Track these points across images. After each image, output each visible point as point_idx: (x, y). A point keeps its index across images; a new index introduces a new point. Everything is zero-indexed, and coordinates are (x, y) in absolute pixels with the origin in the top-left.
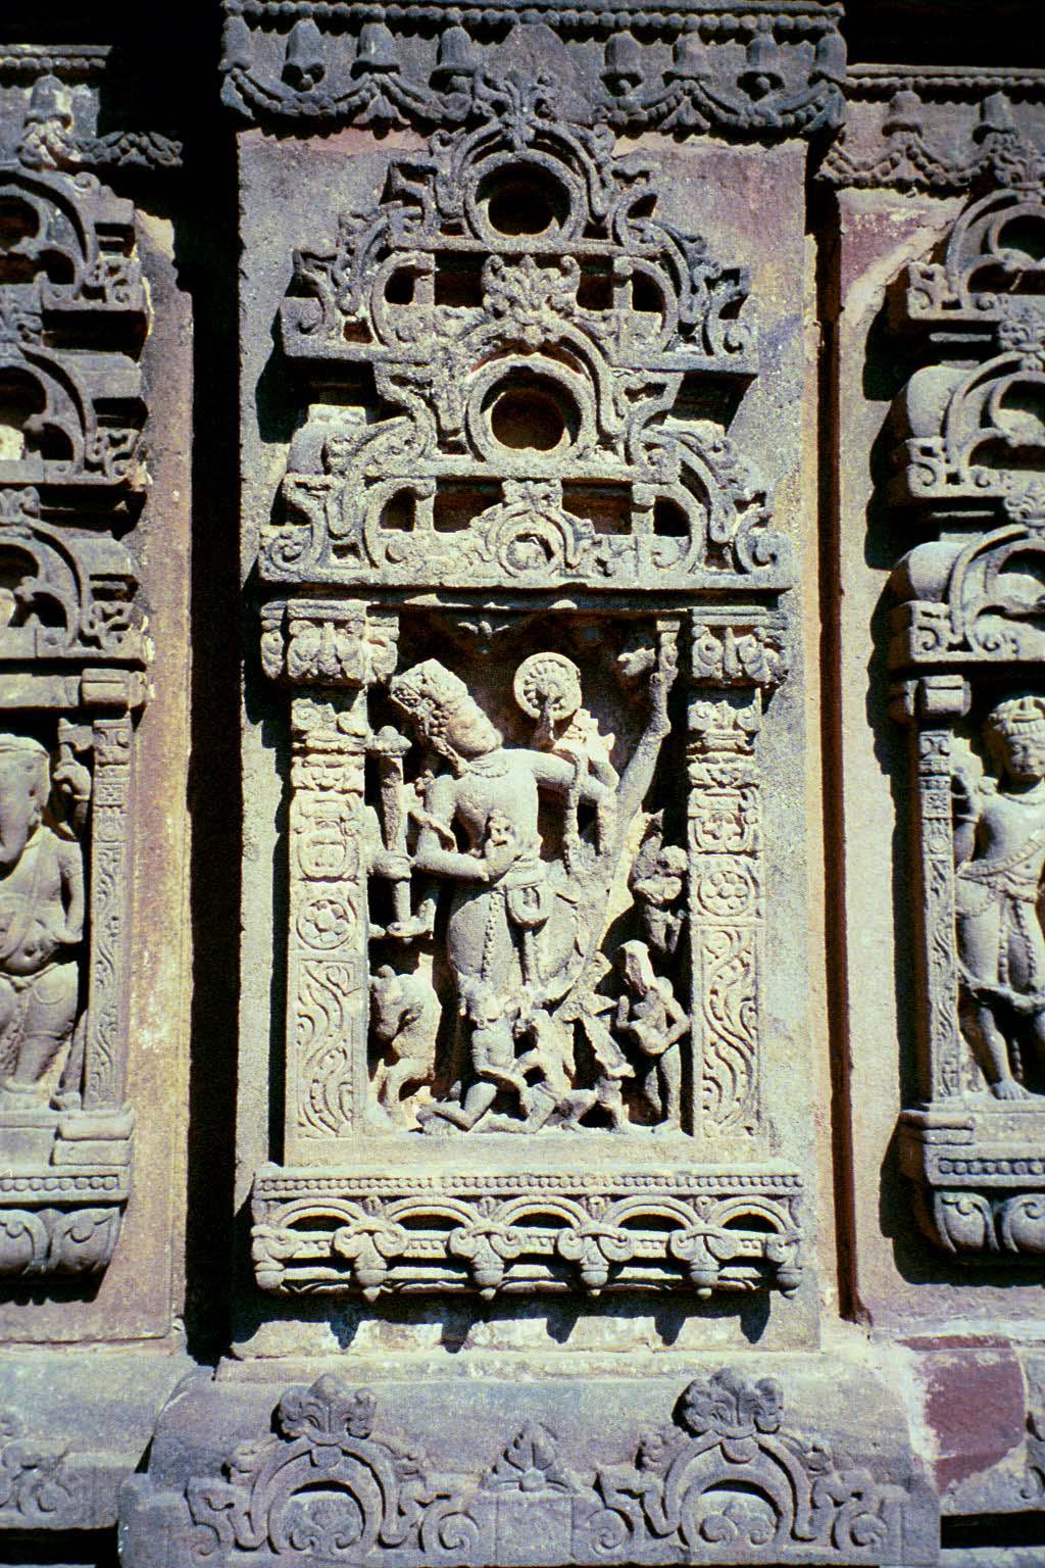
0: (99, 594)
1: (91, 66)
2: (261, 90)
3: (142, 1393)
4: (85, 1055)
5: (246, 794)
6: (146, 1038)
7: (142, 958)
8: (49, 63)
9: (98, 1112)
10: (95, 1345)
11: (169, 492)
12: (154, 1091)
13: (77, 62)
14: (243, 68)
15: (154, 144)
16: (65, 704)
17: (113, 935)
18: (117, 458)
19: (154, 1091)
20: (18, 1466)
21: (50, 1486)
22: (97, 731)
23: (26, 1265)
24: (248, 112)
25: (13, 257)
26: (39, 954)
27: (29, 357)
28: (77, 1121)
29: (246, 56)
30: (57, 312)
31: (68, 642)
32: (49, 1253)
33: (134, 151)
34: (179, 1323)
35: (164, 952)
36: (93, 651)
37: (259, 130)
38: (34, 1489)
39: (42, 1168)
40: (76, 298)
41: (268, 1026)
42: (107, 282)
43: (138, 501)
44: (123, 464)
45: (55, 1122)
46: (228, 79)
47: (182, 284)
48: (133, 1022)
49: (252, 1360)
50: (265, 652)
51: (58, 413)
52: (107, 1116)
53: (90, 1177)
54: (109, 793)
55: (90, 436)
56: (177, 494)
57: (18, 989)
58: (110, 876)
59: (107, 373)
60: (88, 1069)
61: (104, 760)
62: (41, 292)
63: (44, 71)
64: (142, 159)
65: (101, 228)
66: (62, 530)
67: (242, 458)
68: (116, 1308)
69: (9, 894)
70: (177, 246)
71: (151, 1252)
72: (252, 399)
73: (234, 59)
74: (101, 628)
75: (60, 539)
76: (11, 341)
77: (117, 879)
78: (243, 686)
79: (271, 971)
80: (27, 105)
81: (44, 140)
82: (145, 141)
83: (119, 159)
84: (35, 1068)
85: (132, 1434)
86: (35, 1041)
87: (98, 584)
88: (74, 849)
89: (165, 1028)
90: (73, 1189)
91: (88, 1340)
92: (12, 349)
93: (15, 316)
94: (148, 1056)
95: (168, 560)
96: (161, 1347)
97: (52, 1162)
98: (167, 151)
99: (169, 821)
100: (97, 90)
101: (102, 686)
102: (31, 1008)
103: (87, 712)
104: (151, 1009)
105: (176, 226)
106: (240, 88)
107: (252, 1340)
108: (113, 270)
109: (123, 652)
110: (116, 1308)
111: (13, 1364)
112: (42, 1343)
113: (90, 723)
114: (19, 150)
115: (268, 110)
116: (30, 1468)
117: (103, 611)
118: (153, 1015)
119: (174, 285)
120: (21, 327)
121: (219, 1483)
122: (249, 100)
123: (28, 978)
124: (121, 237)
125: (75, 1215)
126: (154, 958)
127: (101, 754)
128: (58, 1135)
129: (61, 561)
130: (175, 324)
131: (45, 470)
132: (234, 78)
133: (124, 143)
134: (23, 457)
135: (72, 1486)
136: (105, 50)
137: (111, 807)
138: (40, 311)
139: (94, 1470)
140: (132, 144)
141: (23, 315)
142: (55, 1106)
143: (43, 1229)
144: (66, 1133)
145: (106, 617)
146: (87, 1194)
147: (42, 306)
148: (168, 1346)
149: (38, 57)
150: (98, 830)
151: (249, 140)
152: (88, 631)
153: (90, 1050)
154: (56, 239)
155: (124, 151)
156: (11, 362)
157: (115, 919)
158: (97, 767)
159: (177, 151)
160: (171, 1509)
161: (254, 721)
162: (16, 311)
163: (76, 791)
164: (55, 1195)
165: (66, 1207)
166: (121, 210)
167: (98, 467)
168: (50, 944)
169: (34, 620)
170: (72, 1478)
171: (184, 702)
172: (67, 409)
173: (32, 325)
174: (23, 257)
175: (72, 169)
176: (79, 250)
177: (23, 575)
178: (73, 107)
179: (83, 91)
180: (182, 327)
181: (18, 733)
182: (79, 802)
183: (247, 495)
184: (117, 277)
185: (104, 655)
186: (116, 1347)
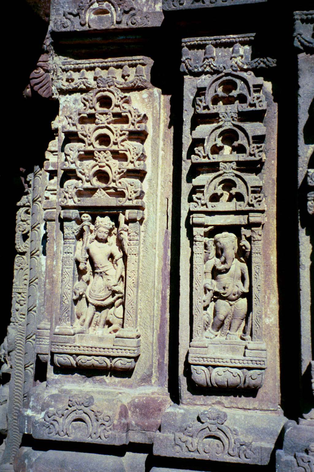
0: (253, 192)
1: (250, 40)
2: (306, 41)
3: (273, 426)
4: (252, 325)
5: (301, 250)
6: (267, 321)
7: (265, 298)
8: (238, 40)
9: (256, 342)
10: (256, 411)
11: (271, 161)
12: (270, 337)
13: (246, 39)
14: (300, 35)
15: (268, 61)
16: (243, 223)
17: (259, 290)
18: (259, 152)
19: (270, 337)
20: (239, 444)
21: (248, 451)
22: (252, 231)
23: (238, 385)
24: (302, 48)
25: (230, 96)
26: (237, 295)
27: (234, 125)
28: (251, 345)
29: (301, 31)
30: (242, 112)
31: (245, 206)
32: (245, 382)
33: (262, 63)
34: (279, 407)
35: (272, 296)
36: (251, 208)
37: (305, 53)
38: (244, 451)
39: (242, 357)
40: (247, 107)
41: (310, 319)
42: (256, 101)
43: (261, 163)
44: (260, 154)
45: (244, 344)
46: (296, 39)
47: (275, 101)
48: (263, 316)
49: (309, 419)
50: (309, 207)
51: (242, 141)
52: (260, 343)
53: (256, 361)
54: (257, 248)
55: (251, 147)
56: (273, 162)
57: (231, 305)
58: (257, 273)
59: (254, 128)
60: (253, 329)
61: (255, 239)
62: (238, 106)
63: (236, 42)
64: (264, 66)
65: (254, 86)
66: (242, 174)
67: (299, 149)
68: (262, 401)
69: (228, 278)
70: (273, 89)
71: (271, 383)
72: (302, 132)
73: (298, 33)
74: (254, 202)
75: (242, 176)
76: (229, 121)
77: (259, 274)
78: (299, 217)
79: (310, 303)
80: (231, 53)
81: (236, 63)
82: (265, 60)
83: (257, 66)
84: (236, 328)
85: (271, 438)
86: (236, 320)
87: (253, 189)
88: (245, 266)
89: (273, 319)
90: (251, 364)
91: (255, 409)
92: (230, 123)
93: (230, 114)
94: (268, 326)
95: (270, 181)
96: (276, 413)
97: (244, 355)
98: (272, 62)
99: (272, 258)
100: (251, 47)
101: (254, 218)
102: (234, 310)
103: (250, 226)
104: (268, 313)
105: (272, 83)
106: (299, 41)
107: (309, 413)
108: (258, 98)
109: (260, 208)
110: (262, 401)
111: (234, 414)
112: (241, 409)
113: (251, 229)
114: (232, 66)
115: (308, 47)
116: (242, 445)
117: (255, 197)
118: (269, 315)
119: (273, 101)
120: (232, 117)
121: (305, 455)
122: (302, 44)
123: (234, 302)
124: (259, 88)
125: (252, 372)
126: (269, 298)
127: (254, 238)
128: (246, 348)
129: (242, 183)
130: (273, 113)
131: (238, 157)
132: (298, 38)
133: (259, 61)
134: (231, 153)
135: (254, 452)
136: (254, 34)
137: (257, 253)
138: (237, 112)
139: (261, 448)
140: (261, 61)
141: (233, 114)
142: (243, 339)
143: (243, 375)
144: (249, 347)
145: (256, 198)
146: (255, 366)
147: (238, 110)
148: (278, 413)
149: (234, 38)
150: (253, 259)
151: (302, 56)
152: (250, 203)
153: (253, 324)
154: (242, 90)
155: (259, 64)
156: (229, 127)
157: (259, 286)
158: (252, 242)
159: (275, 62)
160: (291, 461)
161: (303, 228)
162: (231, 112)
163: (246, 248)
164: (246, 365)
165: (249, 369)
166: (260, 80)
167: (254, 155)
168: (240, 292)
169: (234, 200)
170: (255, 449)
171: (274, 222)
172: (244, 139)
173: (235, 116)
174: (233, 96)
175: (246, 70)
176: (248, 93)
177: (232, 187)
178: (244, 53)
179: (247, 47)
180: (275, 113)
181: (229, 232)
182: (247, 252)
183: (300, 160)
184: (259, 100)
185: (255, 209)
186: (263, 412)
